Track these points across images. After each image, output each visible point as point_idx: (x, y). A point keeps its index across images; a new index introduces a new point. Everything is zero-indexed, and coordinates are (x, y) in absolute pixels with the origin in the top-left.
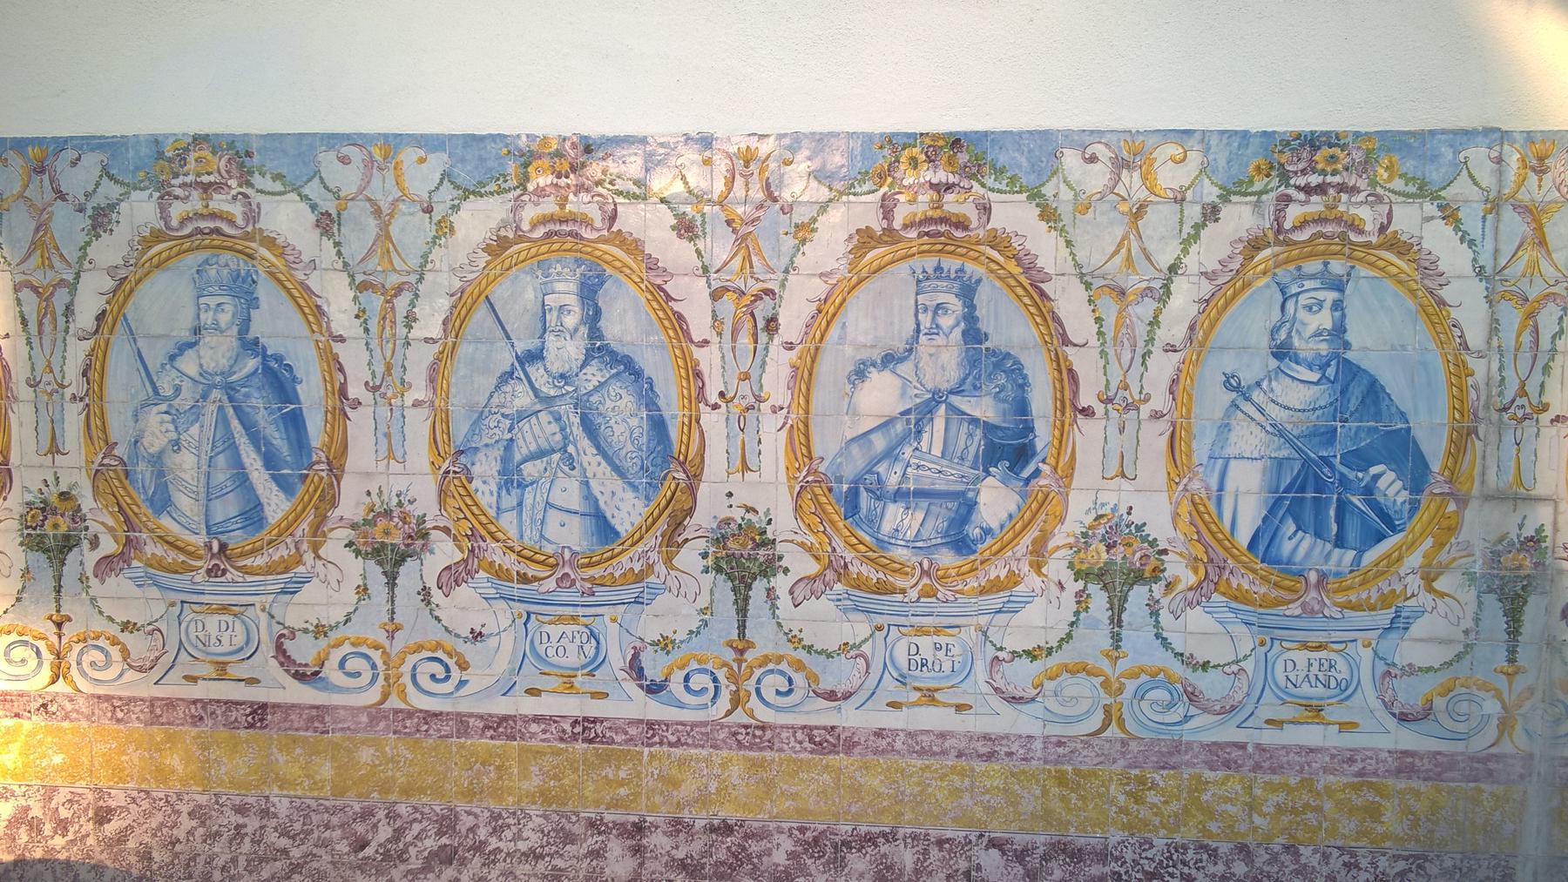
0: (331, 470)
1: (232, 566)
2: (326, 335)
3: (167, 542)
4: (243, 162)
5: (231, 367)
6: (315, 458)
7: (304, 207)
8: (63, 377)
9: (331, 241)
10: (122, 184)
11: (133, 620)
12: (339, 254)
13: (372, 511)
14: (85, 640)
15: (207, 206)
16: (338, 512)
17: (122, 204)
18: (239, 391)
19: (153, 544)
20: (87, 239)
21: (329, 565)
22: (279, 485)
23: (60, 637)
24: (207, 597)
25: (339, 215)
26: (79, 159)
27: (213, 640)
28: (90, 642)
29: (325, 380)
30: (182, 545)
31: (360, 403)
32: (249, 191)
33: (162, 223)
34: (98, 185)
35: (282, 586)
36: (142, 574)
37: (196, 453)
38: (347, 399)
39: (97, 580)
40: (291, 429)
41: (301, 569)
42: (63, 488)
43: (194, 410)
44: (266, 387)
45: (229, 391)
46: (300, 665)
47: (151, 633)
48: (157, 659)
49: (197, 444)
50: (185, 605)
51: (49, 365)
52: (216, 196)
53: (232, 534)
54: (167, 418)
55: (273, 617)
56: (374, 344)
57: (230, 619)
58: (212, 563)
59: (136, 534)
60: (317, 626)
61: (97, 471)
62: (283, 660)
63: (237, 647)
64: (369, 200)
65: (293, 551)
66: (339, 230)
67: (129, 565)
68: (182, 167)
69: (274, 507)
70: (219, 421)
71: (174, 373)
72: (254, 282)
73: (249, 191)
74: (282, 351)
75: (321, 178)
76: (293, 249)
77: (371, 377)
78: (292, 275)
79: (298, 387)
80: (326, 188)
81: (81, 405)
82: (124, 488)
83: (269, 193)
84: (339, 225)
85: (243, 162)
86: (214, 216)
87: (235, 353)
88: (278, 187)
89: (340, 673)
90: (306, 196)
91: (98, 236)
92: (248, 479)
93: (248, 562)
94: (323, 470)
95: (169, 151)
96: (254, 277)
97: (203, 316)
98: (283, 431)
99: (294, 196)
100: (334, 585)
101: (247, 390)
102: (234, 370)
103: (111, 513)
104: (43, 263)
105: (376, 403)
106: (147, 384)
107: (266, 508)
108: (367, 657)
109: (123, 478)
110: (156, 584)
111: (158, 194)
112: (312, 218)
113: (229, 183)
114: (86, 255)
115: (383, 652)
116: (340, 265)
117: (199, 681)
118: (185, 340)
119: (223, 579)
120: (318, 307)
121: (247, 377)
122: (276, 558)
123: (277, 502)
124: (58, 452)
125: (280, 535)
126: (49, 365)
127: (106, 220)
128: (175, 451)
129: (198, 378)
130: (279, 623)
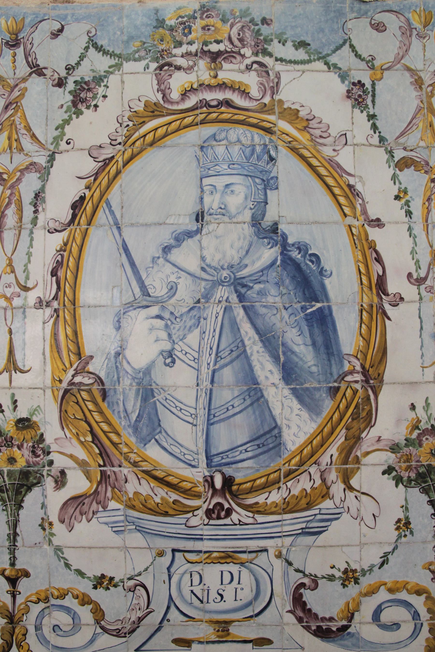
0: (367, 381)
1: (239, 505)
2: (362, 218)
3: (156, 478)
4: (259, 30)
5: (241, 259)
6: (347, 367)
7: (334, 78)
8: (27, 278)
9: (365, 113)
10: (112, 55)
11: (109, 574)
12: (374, 127)
13: (417, 428)
14: (46, 600)
15: (216, 77)
16: (374, 432)
17: (111, 77)
18: (252, 288)
19: (136, 481)
20: (66, 116)
21: (364, 497)
22: (301, 401)
23: (14, 596)
24: (206, 543)
25: (373, 85)
26: (61, 30)
27: (213, 595)
28: (53, 601)
29: (360, 272)
30: (175, 481)
31: (402, 299)
32: (267, 60)
33: (160, 96)
34: (82, 57)
35: (304, 525)
36: (122, 518)
37: (196, 366)
38: (387, 295)
39: (63, 526)
40: (316, 331)
41: (327, 504)
42: (22, 413)
43: (194, 313)
44: (287, 281)
45: (239, 288)
46: (323, 619)
47: (132, 590)
48: (140, 619)
49: (196, 355)
50: (177, 554)
51: (10, 265)
52: (226, 66)
53: (240, 465)
54: (159, 323)
55: (290, 564)
56: (418, 229)
57: (234, 568)
58: (213, 502)
59: (116, 469)
60: (346, 572)
61: (66, 392)
62: (301, 614)
63: (244, 601)
64: (408, 69)
65: (318, 482)
66: (373, 102)
67: (105, 508)
68: (186, 35)
69: (294, 429)
70: (226, 322)
71: (169, 268)
72: (272, 159)
73: (267, 60)
74: (306, 238)
75: (352, 46)
76: (320, 122)
77: (414, 267)
78: (318, 151)
79: (327, 282)
80: (358, 56)
81: (48, 311)
82: (101, 412)
83: (290, 62)
84: (374, 96)
85: (259, 30)
86: (223, 86)
87: (246, 243)
88: (301, 55)
89: (375, 628)
90: (335, 66)
91: (79, 113)
92: (262, 396)
93: (261, 499)
94: (356, 382)
95: (171, 19)
96: (273, 153)
97: (207, 200)
98: (307, 334)
99: (319, 65)
100: (370, 521)
101: (262, 286)
102: (246, 261)
103: (82, 443)
104: (10, 147)
105: (421, 299)
106: (134, 284)
107: (285, 430)
108: (407, 604)
109: (99, 399)
110: (140, 529)
111: (155, 65)
112: (343, 88)
113: (242, 51)
114: (63, 134)
115: (427, 598)
116: (375, 140)
117: (194, 646)
118: (183, 228)
119: (227, 521)
120: (350, 187)
121: (262, 271)
122: (296, 492)
123: (299, 423)
124: (17, 369)
125: (301, 463)
126: (10, 265)
127: (90, 95)
128: (166, 365)
129: (199, 273)
130: (297, 571)
